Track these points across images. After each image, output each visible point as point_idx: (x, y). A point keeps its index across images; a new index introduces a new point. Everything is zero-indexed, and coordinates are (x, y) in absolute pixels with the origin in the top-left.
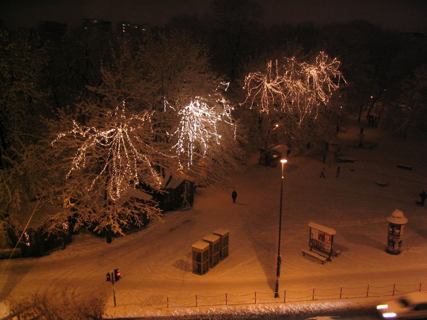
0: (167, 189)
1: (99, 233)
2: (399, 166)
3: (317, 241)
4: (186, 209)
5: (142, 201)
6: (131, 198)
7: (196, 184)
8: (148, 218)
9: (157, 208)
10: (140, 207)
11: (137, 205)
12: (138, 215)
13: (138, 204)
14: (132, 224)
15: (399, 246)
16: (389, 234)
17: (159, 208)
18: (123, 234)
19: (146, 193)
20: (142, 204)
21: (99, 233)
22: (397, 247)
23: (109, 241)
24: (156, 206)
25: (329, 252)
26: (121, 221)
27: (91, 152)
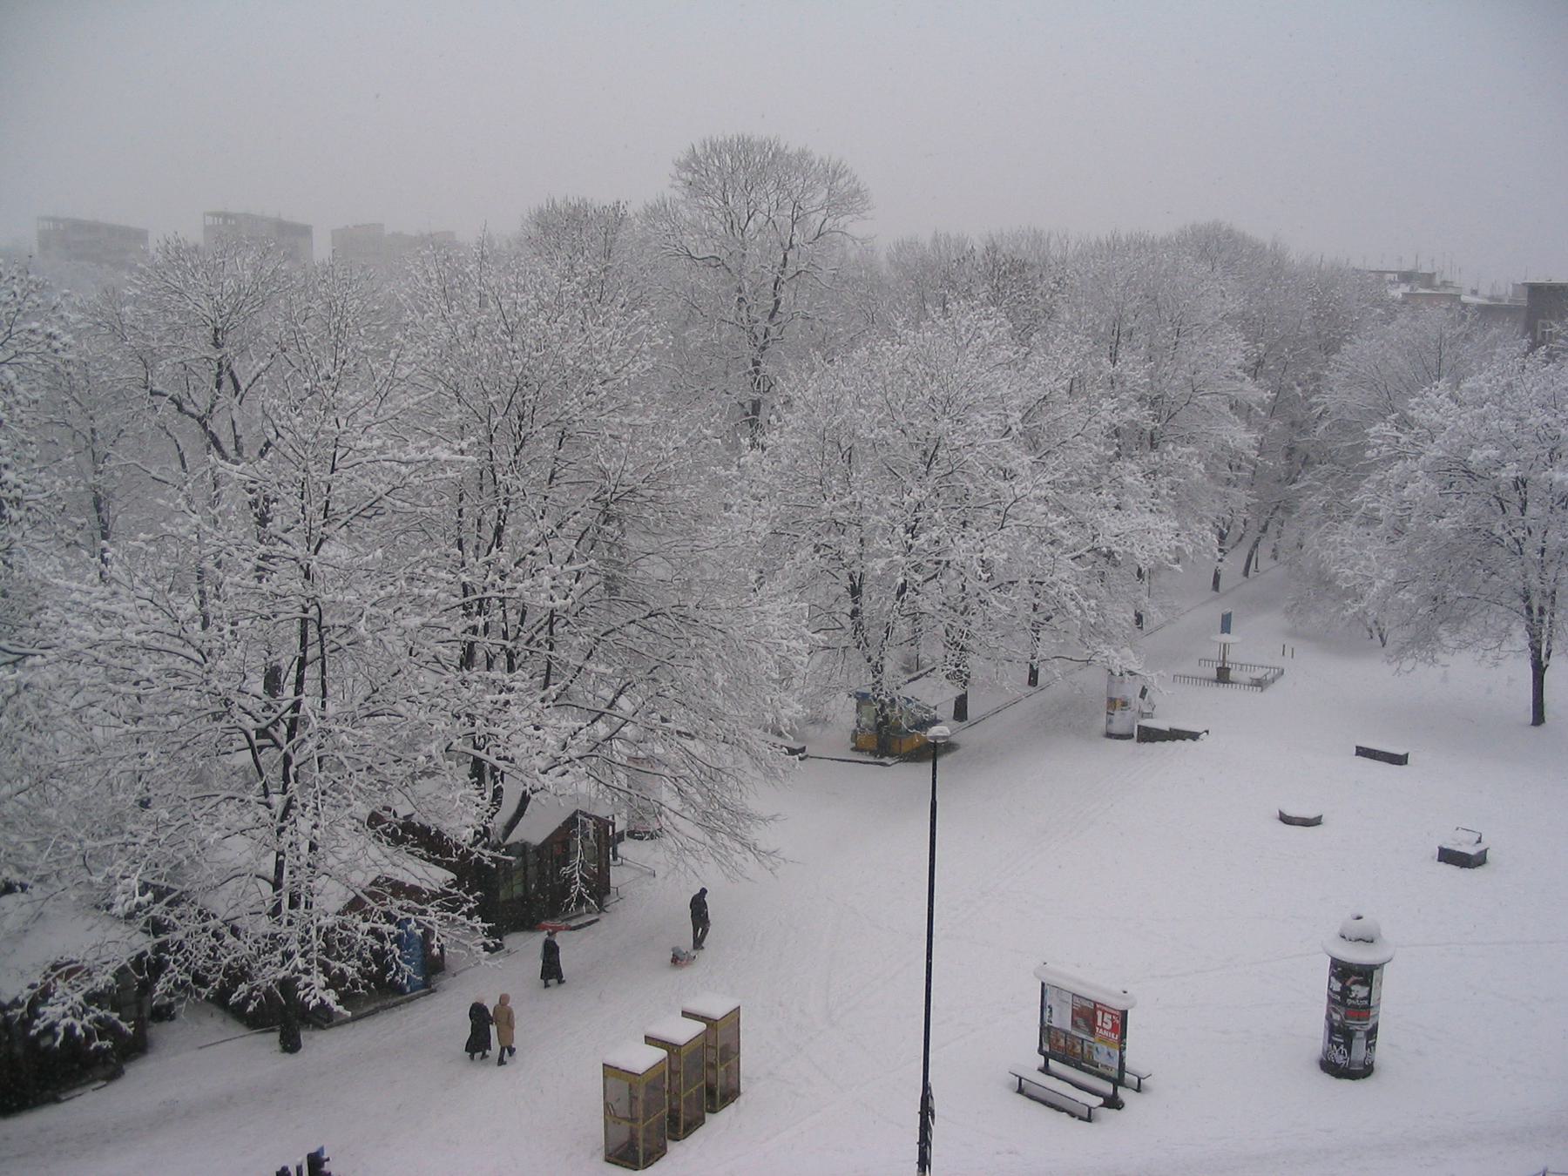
0: (508, 847)
1: (250, 1009)
2: (1362, 752)
3: (1067, 1033)
4: (580, 921)
5: (414, 892)
6: (375, 883)
7: (620, 826)
8: (436, 951)
9: (469, 916)
10: (408, 915)
11: (395, 905)
12: (398, 940)
13: (399, 903)
14: (378, 979)
15: (1368, 1046)
16: (1331, 1000)
17: (477, 918)
18: (340, 1008)
19: (429, 860)
20: (413, 904)
21: (250, 1009)
22: (1359, 1051)
23: (291, 1045)
24: (465, 909)
25: (1114, 1074)
26: (336, 965)
27: (224, 709)
